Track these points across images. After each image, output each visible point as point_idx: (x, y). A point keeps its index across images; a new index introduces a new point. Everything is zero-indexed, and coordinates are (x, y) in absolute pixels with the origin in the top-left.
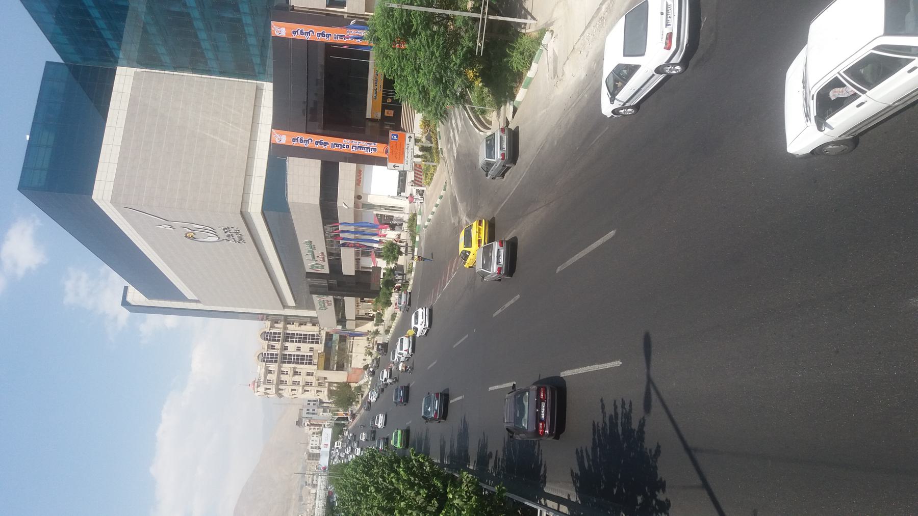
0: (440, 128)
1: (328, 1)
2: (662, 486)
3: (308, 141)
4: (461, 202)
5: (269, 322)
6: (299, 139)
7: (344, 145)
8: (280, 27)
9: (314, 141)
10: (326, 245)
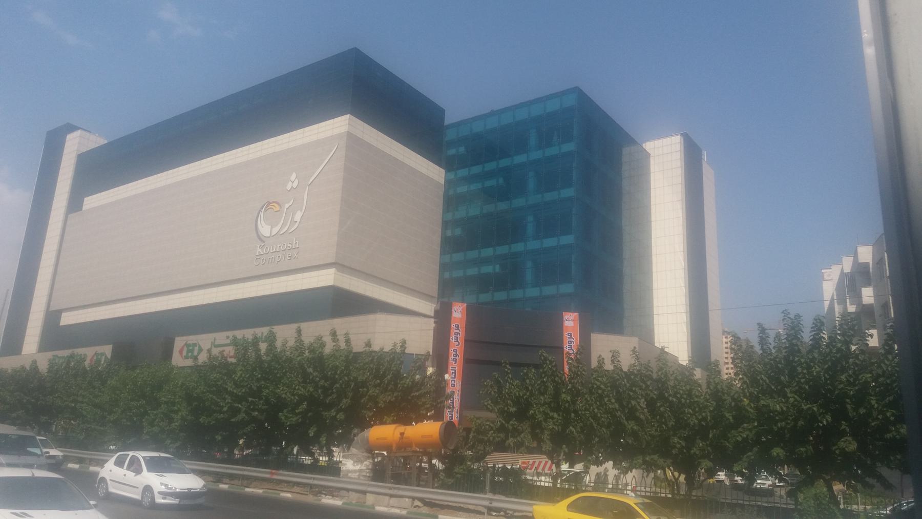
0: (622, 476)
1: (3, 422)
2: (608, 462)
3: (457, 341)
4: (838, 304)
5: (613, 369)
6: (458, 331)
7: (455, 381)
8: (574, 320)
9: (455, 347)
10: (416, 354)
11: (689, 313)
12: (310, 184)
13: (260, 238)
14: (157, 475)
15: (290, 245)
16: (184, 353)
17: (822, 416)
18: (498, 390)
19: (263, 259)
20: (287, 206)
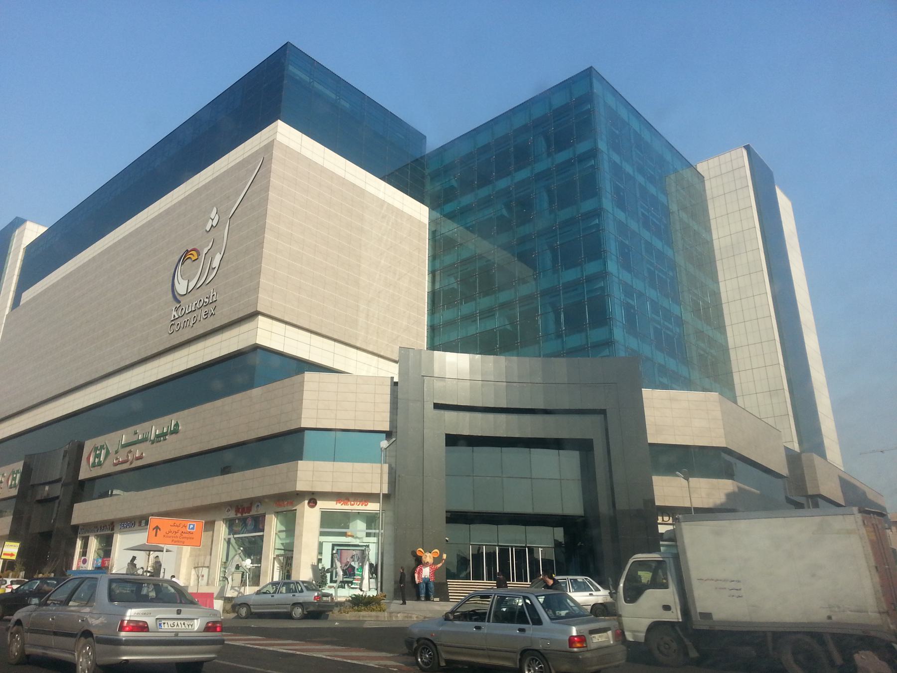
11: (580, 481)
12: (231, 217)
13: (176, 298)
14: (673, 592)
15: (207, 300)
16: (103, 452)
17: (224, 579)
18: (257, 555)
19: (178, 324)
20: (205, 251)
